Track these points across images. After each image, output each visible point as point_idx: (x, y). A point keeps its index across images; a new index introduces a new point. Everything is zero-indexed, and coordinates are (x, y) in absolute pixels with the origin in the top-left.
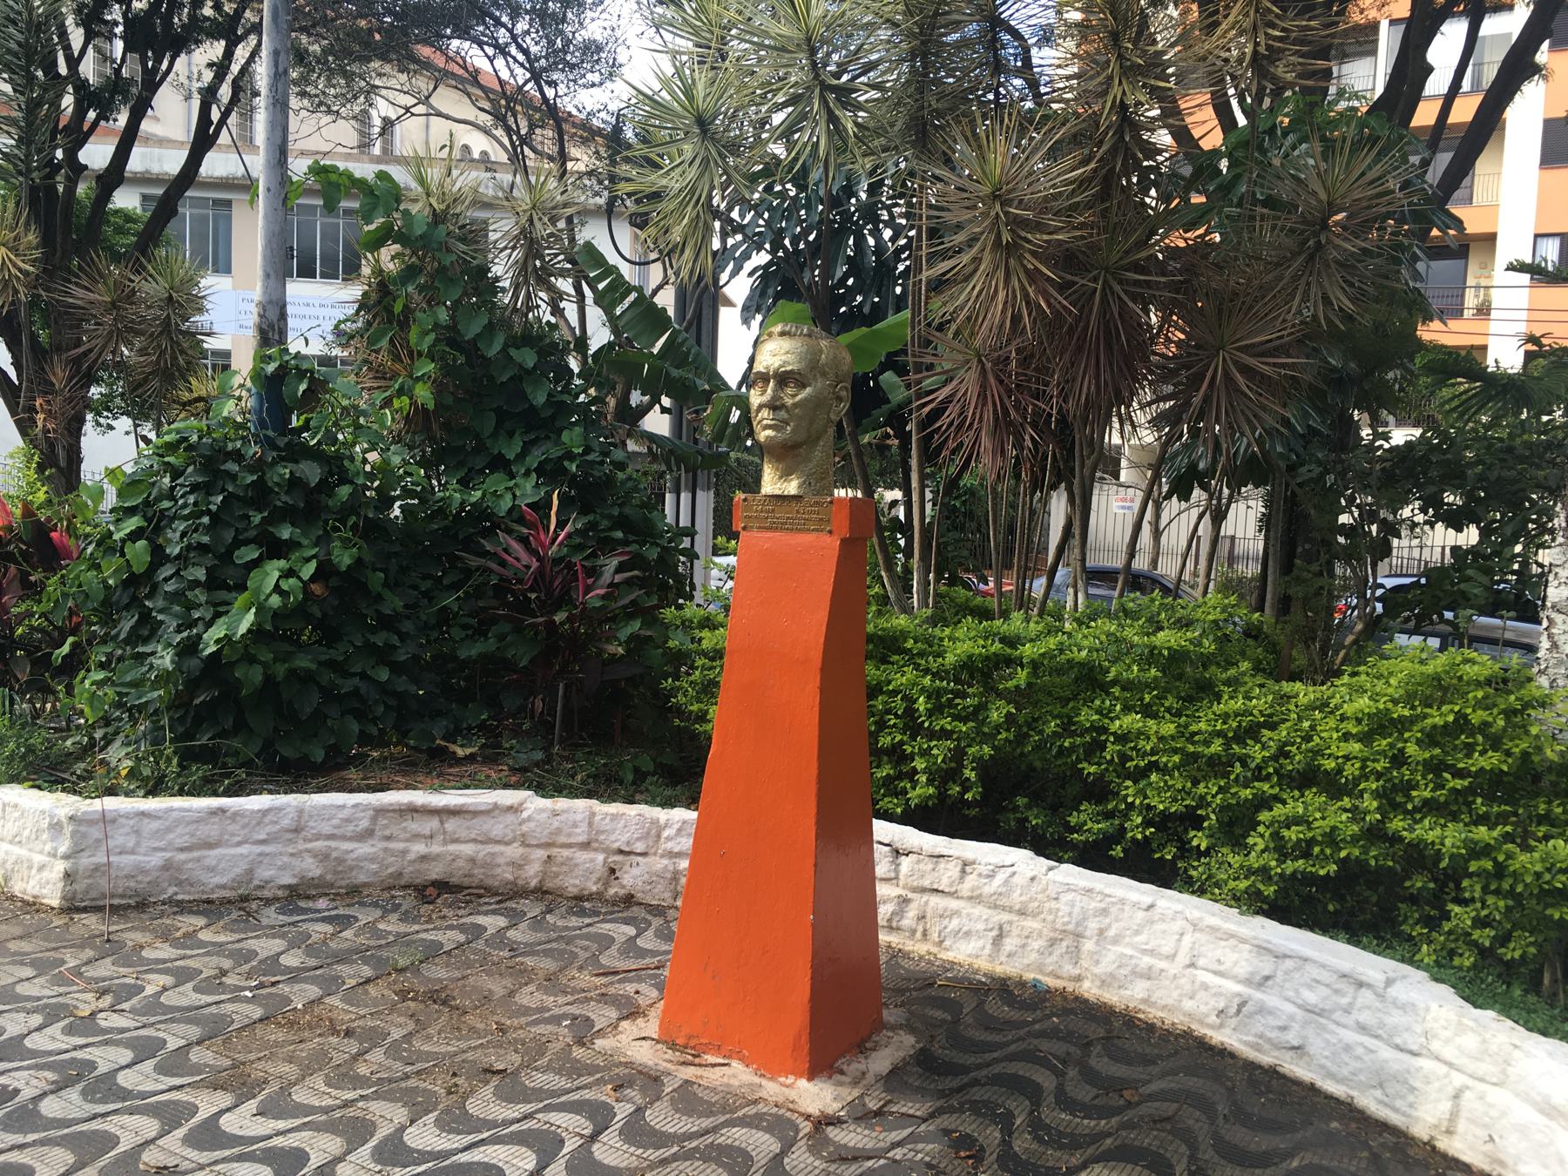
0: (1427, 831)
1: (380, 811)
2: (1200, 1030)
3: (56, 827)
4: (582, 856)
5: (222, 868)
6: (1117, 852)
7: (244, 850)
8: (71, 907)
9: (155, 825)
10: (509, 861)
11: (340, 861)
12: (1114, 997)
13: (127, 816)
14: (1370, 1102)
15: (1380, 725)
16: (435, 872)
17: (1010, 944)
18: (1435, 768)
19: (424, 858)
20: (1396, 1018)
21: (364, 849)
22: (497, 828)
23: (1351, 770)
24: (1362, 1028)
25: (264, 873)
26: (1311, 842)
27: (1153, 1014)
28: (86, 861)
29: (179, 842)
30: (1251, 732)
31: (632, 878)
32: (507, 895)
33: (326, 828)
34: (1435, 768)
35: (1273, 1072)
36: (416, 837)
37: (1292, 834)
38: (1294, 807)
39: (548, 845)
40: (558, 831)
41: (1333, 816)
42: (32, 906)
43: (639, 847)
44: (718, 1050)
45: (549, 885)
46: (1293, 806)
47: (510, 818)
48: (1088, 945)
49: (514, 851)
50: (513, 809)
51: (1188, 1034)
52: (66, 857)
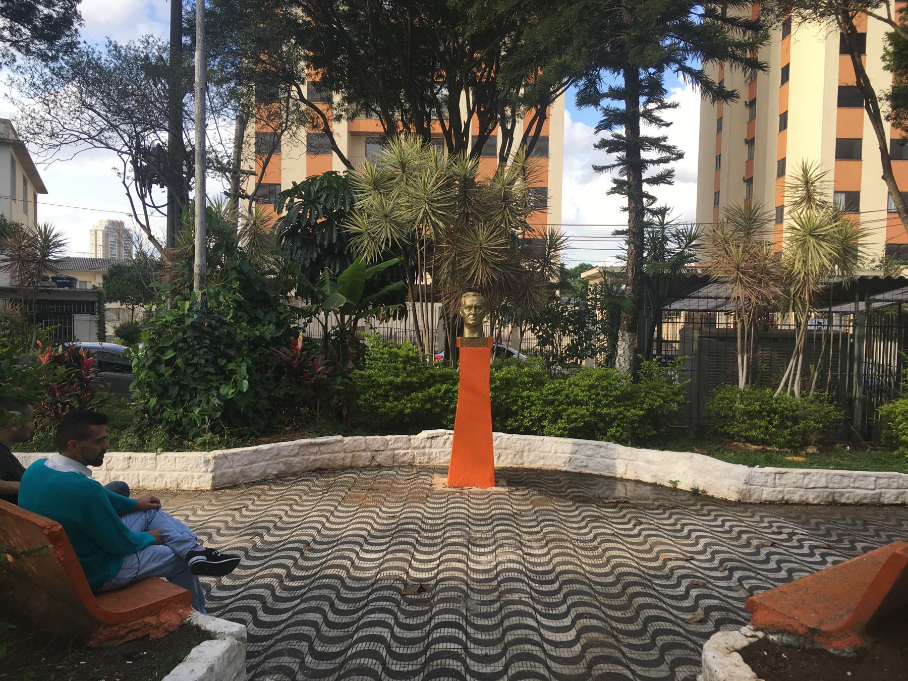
1: (301, 446)
2: (559, 468)
3: (207, 462)
4: (363, 454)
5: (258, 469)
6: (522, 430)
7: (263, 463)
8: (215, 488)
9: (238, 457)
11: (290, 464)
12: (534, 466)
13: (230, 455)
14: (605, 473)
15: (592, 387)
16: (318, 465)
19: (314, 460)
20: (610, 452)
21: (297, 459)
23: (586, 399)
24: (602, 457)
25: (269, 471)
26: (578, 418)
27: (546, 468)
28: (218, 472)
29: (245, 463)
30: (558, 393)
31: (380, 458)
32: (344, 469)
33: (286, 453)
35: (580, 474)
36: (312, 453)
37: (574, 416)
38: (570, 411)
39: (352, 452)
40: (356, 446)
42: (198, 492)
43: (382, 448)
44: (468, 485)
45: (353, 464)
47: (340, 444)
48: (525, 454)
49: (342, 455)
50: (341, 441)
51: (556, 470)
52: (212, 472)
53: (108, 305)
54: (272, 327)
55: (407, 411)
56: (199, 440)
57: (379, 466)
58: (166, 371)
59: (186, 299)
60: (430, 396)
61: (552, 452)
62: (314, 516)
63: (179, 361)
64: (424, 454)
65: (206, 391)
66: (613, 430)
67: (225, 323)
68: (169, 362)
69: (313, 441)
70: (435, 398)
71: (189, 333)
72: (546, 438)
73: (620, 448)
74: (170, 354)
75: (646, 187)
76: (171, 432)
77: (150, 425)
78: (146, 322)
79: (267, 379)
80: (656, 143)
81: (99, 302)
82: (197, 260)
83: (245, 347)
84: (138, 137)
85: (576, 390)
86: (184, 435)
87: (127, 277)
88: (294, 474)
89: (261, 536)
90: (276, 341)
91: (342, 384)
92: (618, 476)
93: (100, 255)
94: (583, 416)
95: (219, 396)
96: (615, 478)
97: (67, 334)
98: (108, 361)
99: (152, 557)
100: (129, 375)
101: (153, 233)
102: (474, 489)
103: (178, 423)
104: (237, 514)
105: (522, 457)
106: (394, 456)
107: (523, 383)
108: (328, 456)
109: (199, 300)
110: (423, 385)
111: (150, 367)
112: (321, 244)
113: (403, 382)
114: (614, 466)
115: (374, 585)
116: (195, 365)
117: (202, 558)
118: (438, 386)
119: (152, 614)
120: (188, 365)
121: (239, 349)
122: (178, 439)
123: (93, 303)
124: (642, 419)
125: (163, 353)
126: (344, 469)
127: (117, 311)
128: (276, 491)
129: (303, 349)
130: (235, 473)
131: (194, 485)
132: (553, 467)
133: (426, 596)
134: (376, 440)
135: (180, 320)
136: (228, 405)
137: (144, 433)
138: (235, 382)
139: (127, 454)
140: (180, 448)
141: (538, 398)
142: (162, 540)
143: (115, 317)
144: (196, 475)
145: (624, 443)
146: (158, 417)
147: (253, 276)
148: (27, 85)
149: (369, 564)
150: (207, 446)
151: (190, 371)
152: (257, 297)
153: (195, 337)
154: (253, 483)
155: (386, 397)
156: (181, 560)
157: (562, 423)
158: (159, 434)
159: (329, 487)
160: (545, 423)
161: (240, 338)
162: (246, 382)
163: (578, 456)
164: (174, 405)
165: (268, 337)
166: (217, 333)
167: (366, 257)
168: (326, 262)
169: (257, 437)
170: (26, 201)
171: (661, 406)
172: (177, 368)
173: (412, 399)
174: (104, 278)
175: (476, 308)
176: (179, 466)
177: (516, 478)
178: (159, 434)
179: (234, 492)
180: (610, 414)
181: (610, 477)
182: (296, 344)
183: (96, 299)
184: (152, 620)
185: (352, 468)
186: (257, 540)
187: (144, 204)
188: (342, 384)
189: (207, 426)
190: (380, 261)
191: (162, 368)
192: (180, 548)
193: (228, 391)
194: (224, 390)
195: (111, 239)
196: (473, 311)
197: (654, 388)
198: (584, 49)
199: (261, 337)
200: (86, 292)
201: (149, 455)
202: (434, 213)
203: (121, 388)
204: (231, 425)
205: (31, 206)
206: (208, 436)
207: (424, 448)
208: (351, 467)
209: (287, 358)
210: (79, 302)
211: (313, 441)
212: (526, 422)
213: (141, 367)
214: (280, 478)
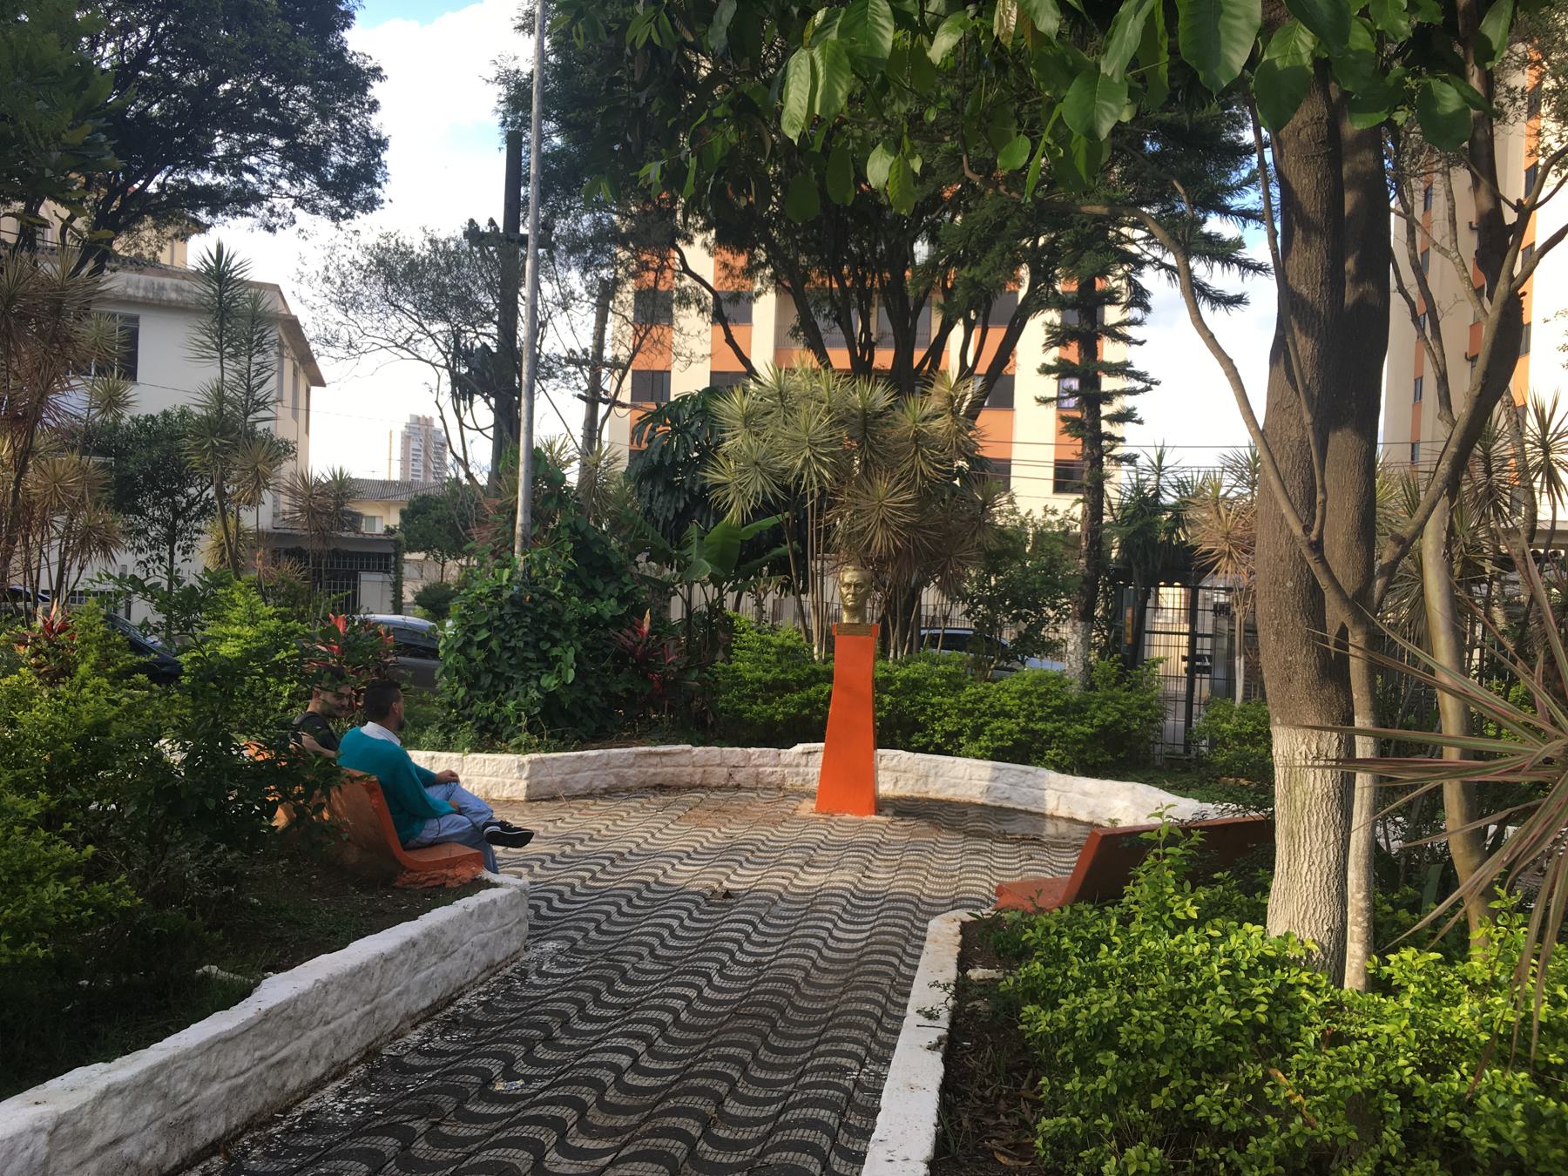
0: (1040, 726)
1: (637, 755)
3: (521, 767)
4: (718, 769)
5: (581, 781)
10: (688, 774)
12: (941, 796)
14: (1032, 808)
15: (1025, 693)
16: (658, 780)
17: (900, 784)
18: (1041, 706)
21: (631, 771)
22: (683, 760)
23: (1015, 709)
27: (956, 799)
28: (535, 780)
30: (981, 700)
31: (739, 777)
32: (692, 787)
34: (1041, 706)
37: (999, 732)
41: (1010, 725)
46: (996, 724)
49: (690, 769)
53: (407, 556)
54: (613, 602)
55: (778, 717)
56: (513, 742)
57: (738, 787)
58: (478, 654)
59: (504, 567)
60: (809, 699)
61: (966, 777)
62: (639, 831)
63: (494, 644)
64: (798, 774)
65: (525, 681)
66: (1052, 753)
67: (552, 597)
68: (482, 645)
69: (653, 749)
70: (816, 701)
71: (507, 609)
72: (958, 760)
73: (1053, 776)
74: (483, 634)
75: (1105, 427)
76: (482, 730)
77: (457, 721)
78: (464, 583)
79: (605, 670)
80: (1122, 369)
81: (396, 555)
82: (520, 518)
83: (575, 628)
84: (457, 335)
85: (1005, 697)
86: (496, 735)
87: (439, 516)
88: (628, 790)
89: (573, 845)
90: (618, 622)
91: (697, 680)
92: (1048, 812)
93: (396, 476)
94: (1011, 732)
95: (539, 688)
96: (1043, 815)
97: (351, 605)
98: (417, 646)
99: (450, 825)
100: (434, 662)
101: (471, 470)
102: (848, 816)
103: (489, 719)
104: (550, 825)
105: (926, 784)
106: (758, 774)
107: (935, 686)
108: (671, 770)
109: (521, 568)
110: (802, 684)
111: (459, 650)
112: (691, 489)
113: (774, 680)
114: (1043, 799)
115: (679, 892)
116: (513, 649)
117: (497, 828)
118: (821, 686)
119: (448, 867)
120: (504, 648)
121: (567, 631)
122: (490, 738)
123: (387, 556)
124: (1091, 739)
125: (475, 633)
126: (692, 787)
127: (420, 565)
128: (602, 805)
129: (651, 632)
130: (553, 782)
131: (505, 794)
132: (966, 799)
133: (729, 901)
134: (735, 753)
135: (497, 592)
136: (550, 698)
137: (451, 730)
138: (559, 671)
139: (430, 754)
140: (492, 749)
141: (952, 706)
142: (460, 812)
143: (416, 574)
144: (508, 782)
145: (1061, 768)
146: (467, 711)
147: (591, 536)
148: (320, 280)
149: (683, 875)
150: (522, 748)
151: (506, 655)
152: (593, 565)
153: (514, 615)
154: (576, 797)
155: (753, 698)
156: (477, 830)
157: (984, 741)
158: (467, 733)
159: (667, 805)
160: (962, 740)
161: (568, 617)
162: (572, 672)
163: (999, 785)
164: (487, 698)
165: (608, 615)
166: (540, 610)
167: (733, 516)
168: (697, 514)
169: (584, 742)
170: (295, 408)
171: (1117, 722)
172: (491, 651)
173: (785, 703)
174: (403, 513)
175: (856, 586)
176: (488, 770)
177: (908, 809)
178: (467, 733)
179: (551, 804)
180: (1044, 731)
181: (1037, 814)
182: (641, 626)
183: (392, 550)
184: (450, 873)
185: (702, 787)
186: (568, 849)
187: (461, 423)
188: (697, 680)
189: (524, 723)
190: (749, 521)
191: (474, 652)
192: (476, 820)
193: (549, 682)
194: (545, 682)
195: (414, 445)
196: (852, 590)
197: (1112, 699)
198: (1007, 255)
199: (598, 616)
200: (376, 541)
201: (455, 755)
202: (819, 461)
203: (425, 680)
204: (552, 725)
205: (302, 414)
206: (524, 736)
207: (798, 766)
208: (702, 786)
209: (630, 643)
210: (369, 555)
211: (653, 749)
212: (938, 739)
213: (449, 650)
214: (609, 793)
